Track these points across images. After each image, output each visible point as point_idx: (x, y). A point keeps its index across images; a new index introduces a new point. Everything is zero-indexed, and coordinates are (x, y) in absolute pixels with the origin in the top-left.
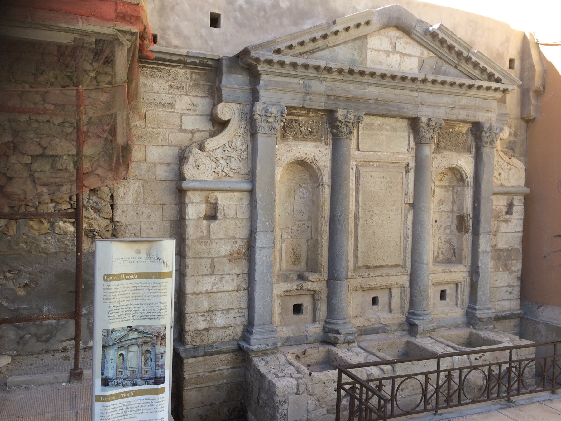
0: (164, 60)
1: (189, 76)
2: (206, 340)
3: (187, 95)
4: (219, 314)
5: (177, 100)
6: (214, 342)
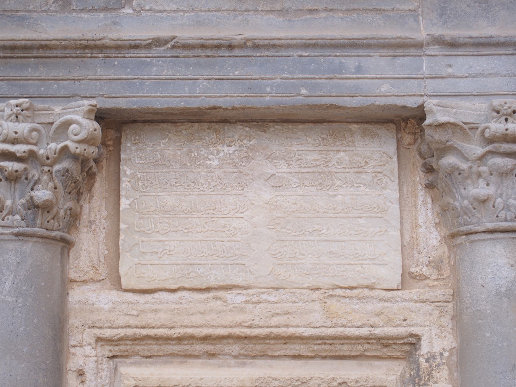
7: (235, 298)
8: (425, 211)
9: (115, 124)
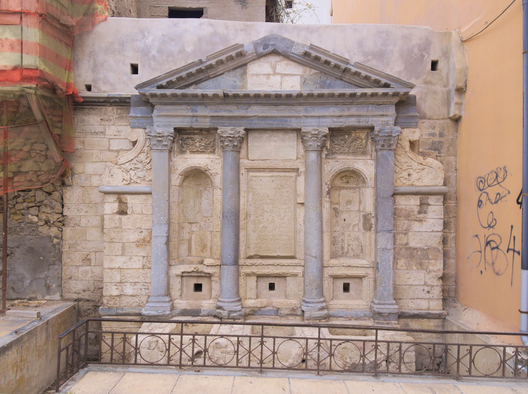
1: (115, 111)
2: (118, 303)
3: (113, 125)
4: (128, 285)
5: (107, 129)
6: (125, 306)
7: (268, 162)
8: (301, 146)
9: (247, 130)
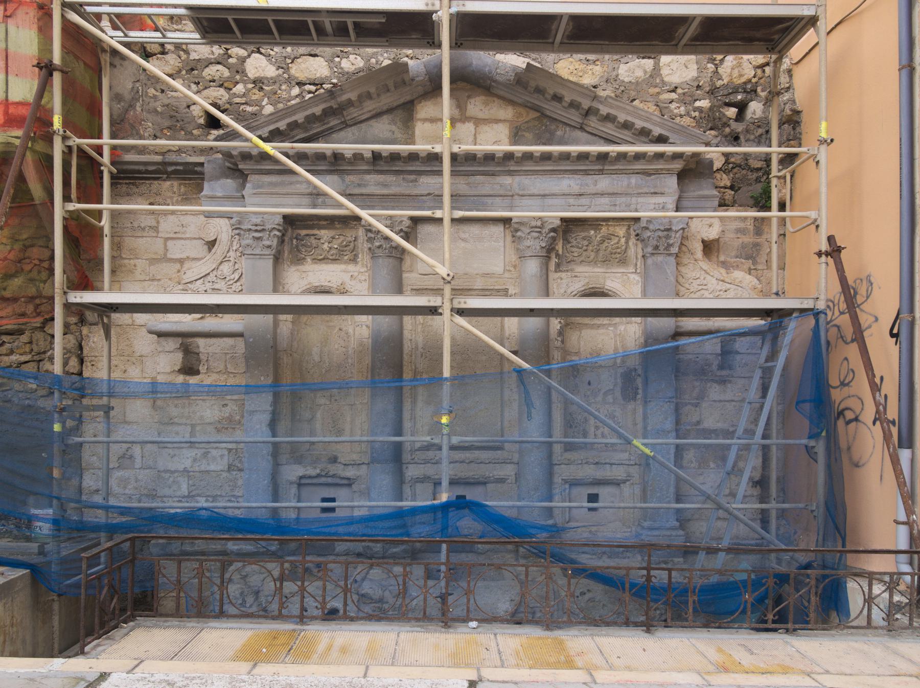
0: (139, 172)
